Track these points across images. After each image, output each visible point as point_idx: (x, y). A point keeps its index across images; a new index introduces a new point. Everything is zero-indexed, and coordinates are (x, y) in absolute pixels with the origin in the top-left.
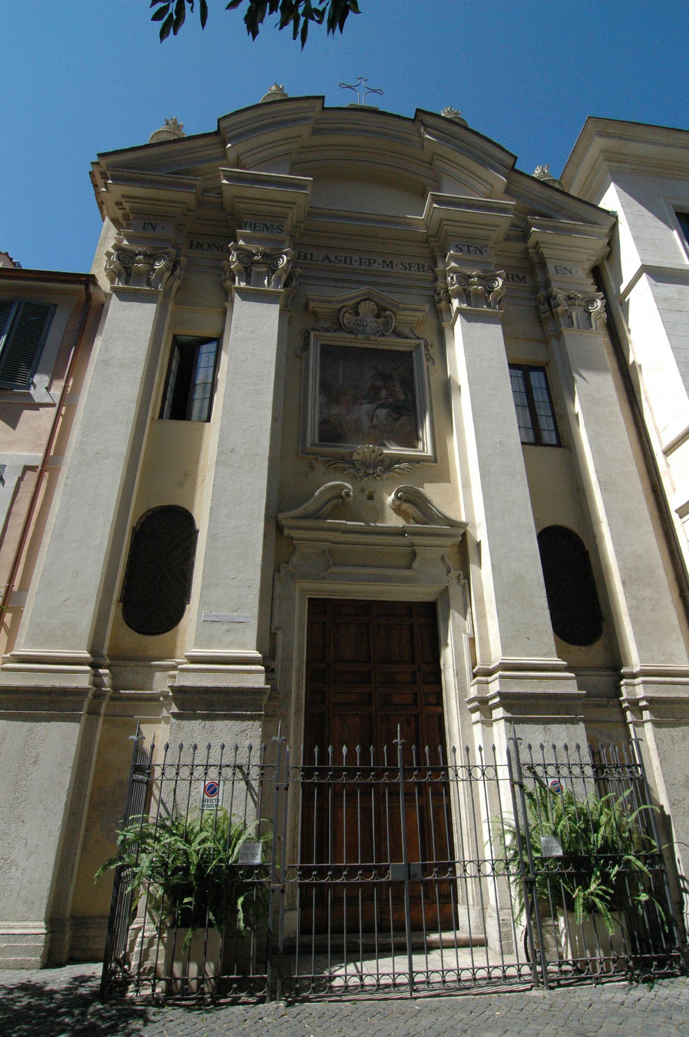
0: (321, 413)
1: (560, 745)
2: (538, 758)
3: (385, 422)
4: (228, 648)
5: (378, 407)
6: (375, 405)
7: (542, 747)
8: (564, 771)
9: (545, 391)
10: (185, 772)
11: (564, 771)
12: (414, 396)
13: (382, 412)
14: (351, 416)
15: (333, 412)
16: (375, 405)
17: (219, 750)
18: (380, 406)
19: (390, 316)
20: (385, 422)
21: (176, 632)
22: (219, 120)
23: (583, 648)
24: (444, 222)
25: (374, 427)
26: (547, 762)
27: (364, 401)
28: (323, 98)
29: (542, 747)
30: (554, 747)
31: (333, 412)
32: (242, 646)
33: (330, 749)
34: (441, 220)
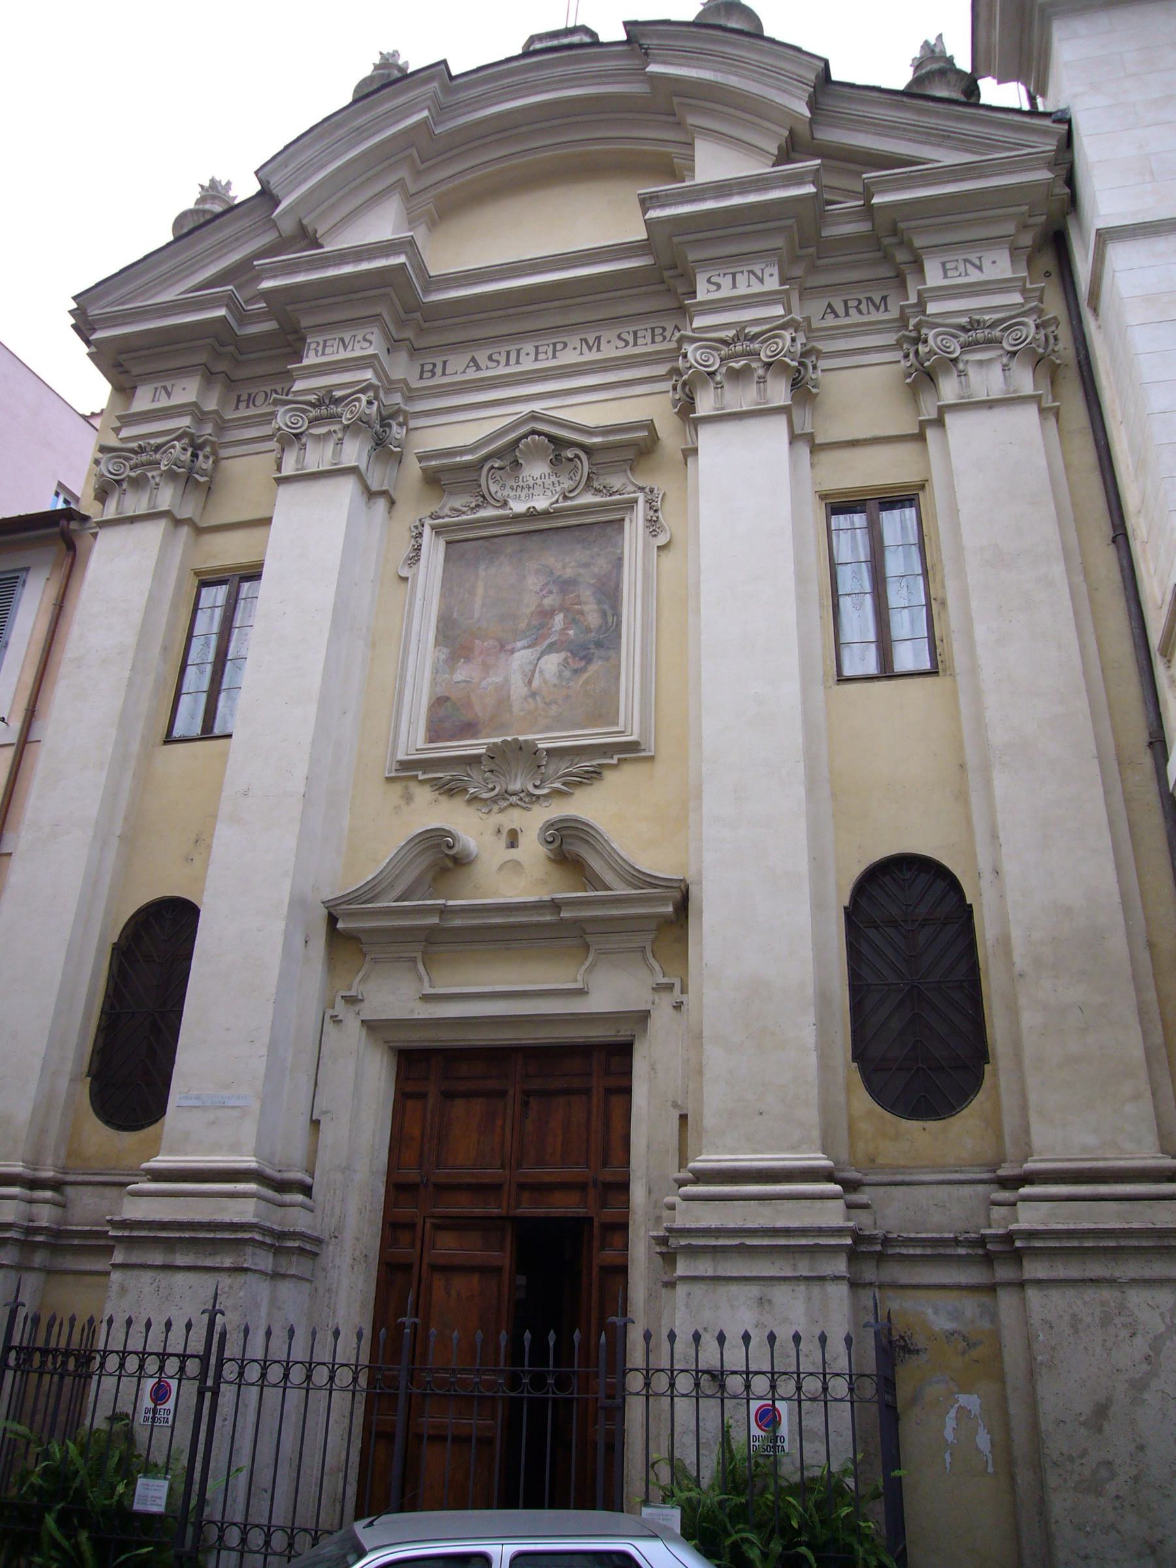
0: (434, 682)
1: (784, 1334)
2: (735, 1358)
3: (555, 681)
4: (210, 1153)
5: (543, 654)
6: (539, 649)
7: (746, 1338)
8: (787, 1387)
9: (915, 551)
10: (132, 1363)
11: (787, 1387)
12: (617, 614)
13: (552, 663)
14: (490, 680)
15: (460, 676)
16: (539, 649)
17: (330, 1338)
18: (551, 648)
19: (577, 456)
20: (555, 681)
21: (163, 1125)
22: (256, 173)
23: (930, 1125)
24: (676, 240)
25: (533, 695)
26: (753, 1368)
27: (519, 644)
28: (444, 62)
29: (746, 1338)
30: (772, 1338)
31: (460, 676)
32: (235, 1148)
33: (552, 1337)
34: (671, 236)
